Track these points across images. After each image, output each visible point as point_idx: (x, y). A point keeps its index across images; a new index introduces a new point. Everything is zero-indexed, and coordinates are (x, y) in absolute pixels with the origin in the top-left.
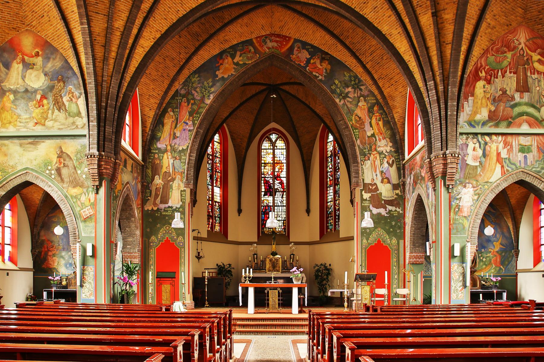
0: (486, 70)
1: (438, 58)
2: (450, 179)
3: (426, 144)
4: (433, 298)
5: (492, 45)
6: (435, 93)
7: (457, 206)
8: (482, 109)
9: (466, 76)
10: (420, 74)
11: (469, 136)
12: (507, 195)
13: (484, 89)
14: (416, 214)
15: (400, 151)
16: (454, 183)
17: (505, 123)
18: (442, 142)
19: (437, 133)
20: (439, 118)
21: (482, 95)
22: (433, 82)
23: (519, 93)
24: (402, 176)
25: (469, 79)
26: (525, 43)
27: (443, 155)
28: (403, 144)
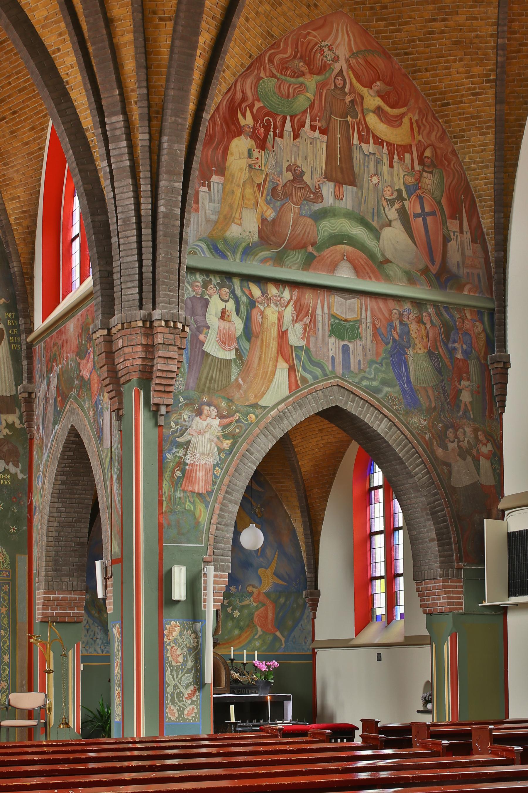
0: (255, 110)
1: (136, 53)
2: (161, 388)
3: (98, 287)
4: (116, 718)
5: (270, 49)
6: (125, 150)
7: (179, 464)
8: (245, 212)
9: (206, 116)
10: (87, 91)
11: (211, 277)
12: (293, 447)
13: (251, 161)
14: (63, 483)
15: (20, 307)
16: (171, 402)
17: (297, 257)
18: (141, 286)
19: (129, 259)
20: (134, 220)
21: (245, 174)
22: (121, 118)
23: (332, 184)
24: (25, 375)
25: (214, 129)
26: (347, 61)
27: (144, 322)
28: (28, 287)
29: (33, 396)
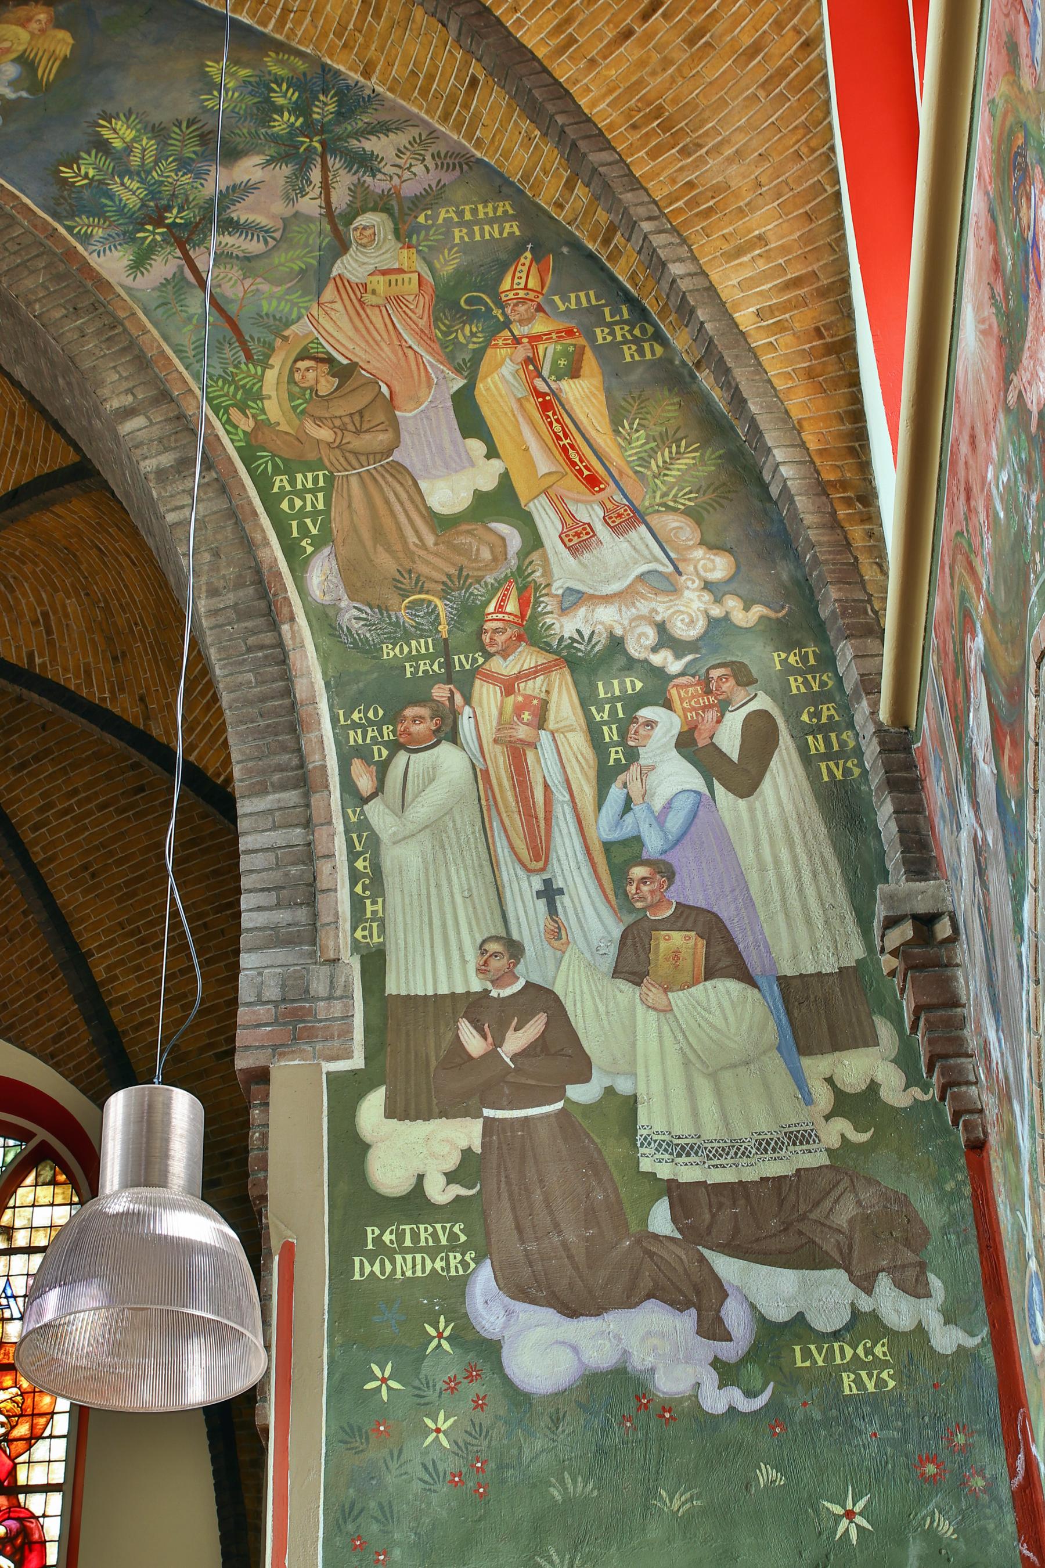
29: (943, 929)
